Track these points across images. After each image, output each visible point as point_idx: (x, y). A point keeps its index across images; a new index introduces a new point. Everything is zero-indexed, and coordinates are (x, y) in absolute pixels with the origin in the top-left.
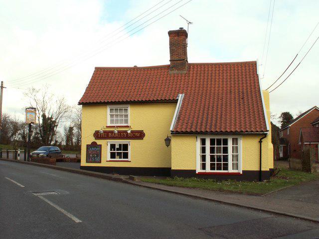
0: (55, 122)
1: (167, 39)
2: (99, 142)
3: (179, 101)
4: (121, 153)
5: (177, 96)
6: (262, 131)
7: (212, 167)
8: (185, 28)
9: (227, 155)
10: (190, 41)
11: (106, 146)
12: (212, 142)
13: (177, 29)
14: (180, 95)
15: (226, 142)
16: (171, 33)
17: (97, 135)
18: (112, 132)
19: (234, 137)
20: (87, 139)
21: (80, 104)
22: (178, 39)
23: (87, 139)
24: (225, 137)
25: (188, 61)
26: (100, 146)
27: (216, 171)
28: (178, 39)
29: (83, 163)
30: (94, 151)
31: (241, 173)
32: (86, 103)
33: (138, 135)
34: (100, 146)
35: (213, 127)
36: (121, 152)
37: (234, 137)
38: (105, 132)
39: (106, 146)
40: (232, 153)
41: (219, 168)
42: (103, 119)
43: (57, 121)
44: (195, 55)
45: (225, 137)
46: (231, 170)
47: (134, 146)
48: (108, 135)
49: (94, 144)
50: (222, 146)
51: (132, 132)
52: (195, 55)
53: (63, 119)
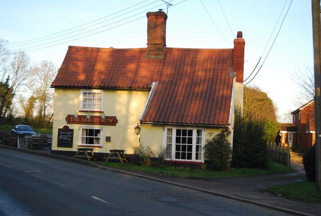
0: (11, 89)
1: (145, 21)
2: (71, 126)
3: (152, 89)
4: (186, 145)
5: (151, 84)
6: (224, 125)
7: (177, 156)
8: (165, 11)
9: (192, 146)
10: (169, 22)
11: (78, 131)
12: (178, 132)
13: (156, 10)
14: (154, 83)
15: (190, 133)
16: (149, 15)
17: (70, 119)
18: (85, 117)
19: (199, 129)
20: (59, 123)
21: (52, 86)
22: (157, 21)
23: (59, 123)
24: (190, 129)
25: (167, 44)
26: (72, 131)
27: (180, 160)
28: (157, 21)
29: (55, 147)
30: (66, 136)
31: (203, 163)
32: (57, 86)
33: (111, 121)
34: (72, 131)
35: (180, 118)
36: (91, 137)
37: (199, 129)
38: (80, 117)
39: (78, 131)
40: (81, 136)
41: (183, 157)
42: (76, 101)
43: (14, 88)
44: (176, 39)
45: (190, 129)
46: (194, 159)
47: (106, 131)
48: (80, 119)
49: (66, 128)
50: (187, 137)
51: (107, 118)
52: (176, 39)
53: (22, 88)
